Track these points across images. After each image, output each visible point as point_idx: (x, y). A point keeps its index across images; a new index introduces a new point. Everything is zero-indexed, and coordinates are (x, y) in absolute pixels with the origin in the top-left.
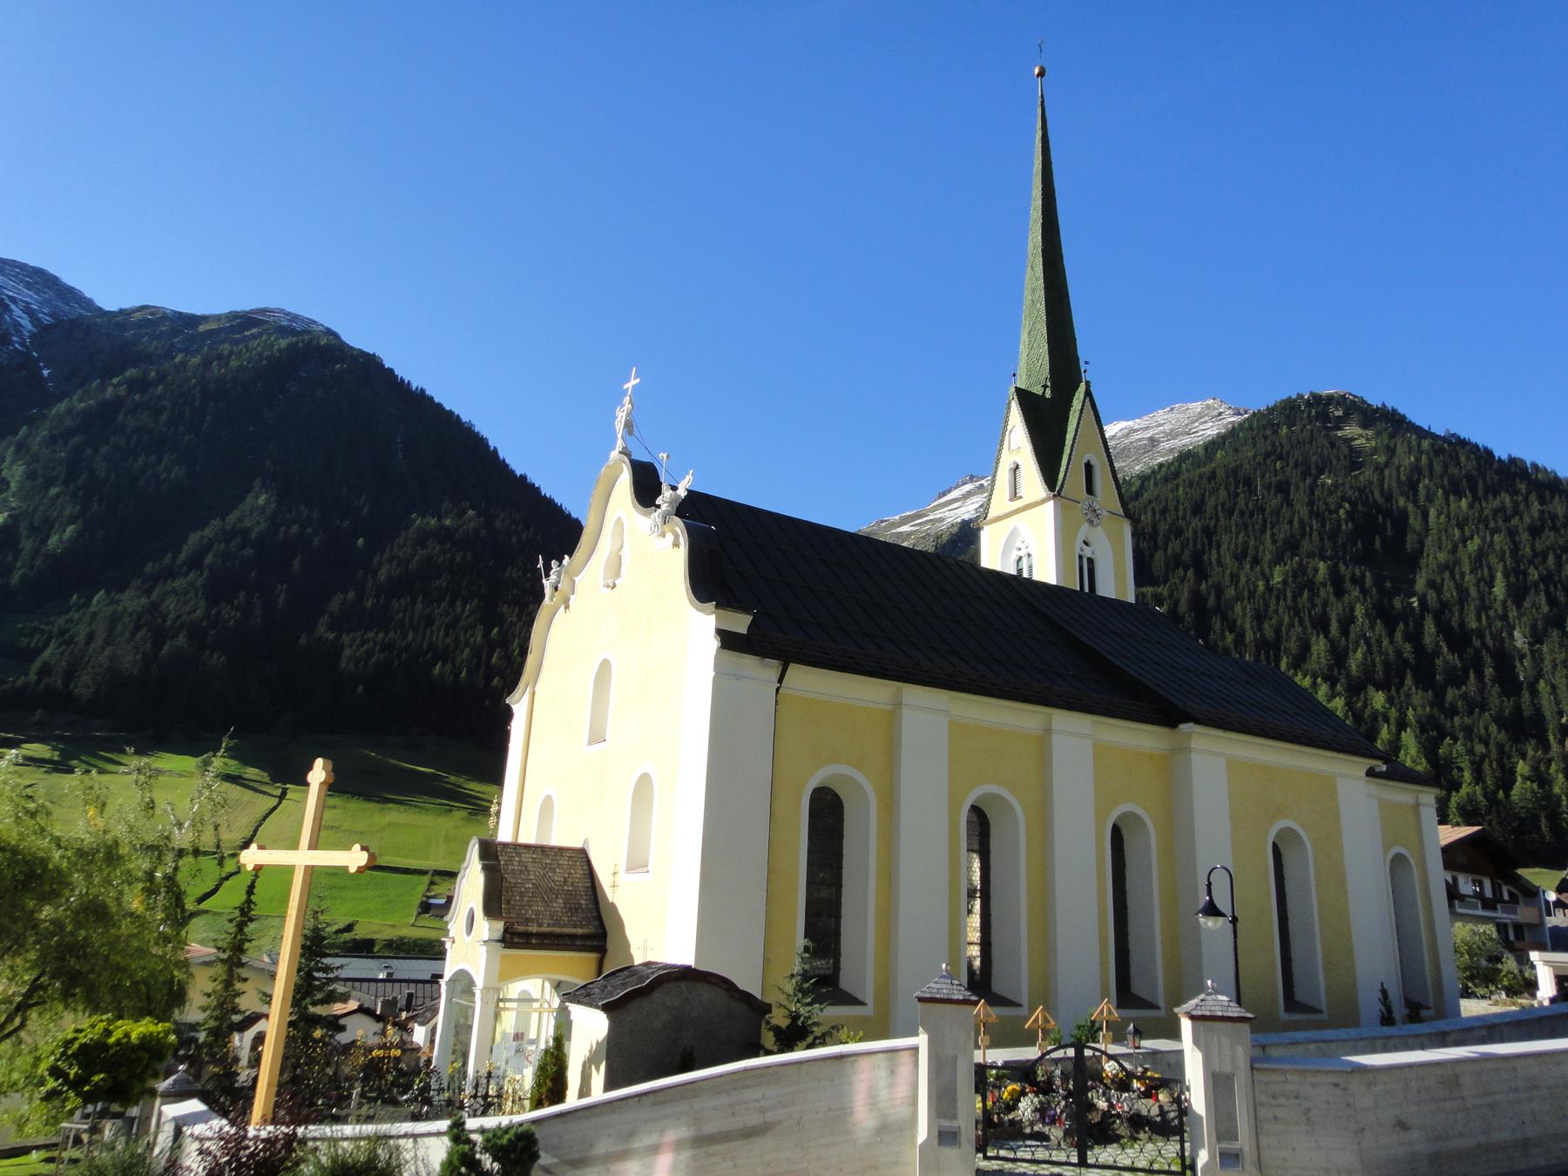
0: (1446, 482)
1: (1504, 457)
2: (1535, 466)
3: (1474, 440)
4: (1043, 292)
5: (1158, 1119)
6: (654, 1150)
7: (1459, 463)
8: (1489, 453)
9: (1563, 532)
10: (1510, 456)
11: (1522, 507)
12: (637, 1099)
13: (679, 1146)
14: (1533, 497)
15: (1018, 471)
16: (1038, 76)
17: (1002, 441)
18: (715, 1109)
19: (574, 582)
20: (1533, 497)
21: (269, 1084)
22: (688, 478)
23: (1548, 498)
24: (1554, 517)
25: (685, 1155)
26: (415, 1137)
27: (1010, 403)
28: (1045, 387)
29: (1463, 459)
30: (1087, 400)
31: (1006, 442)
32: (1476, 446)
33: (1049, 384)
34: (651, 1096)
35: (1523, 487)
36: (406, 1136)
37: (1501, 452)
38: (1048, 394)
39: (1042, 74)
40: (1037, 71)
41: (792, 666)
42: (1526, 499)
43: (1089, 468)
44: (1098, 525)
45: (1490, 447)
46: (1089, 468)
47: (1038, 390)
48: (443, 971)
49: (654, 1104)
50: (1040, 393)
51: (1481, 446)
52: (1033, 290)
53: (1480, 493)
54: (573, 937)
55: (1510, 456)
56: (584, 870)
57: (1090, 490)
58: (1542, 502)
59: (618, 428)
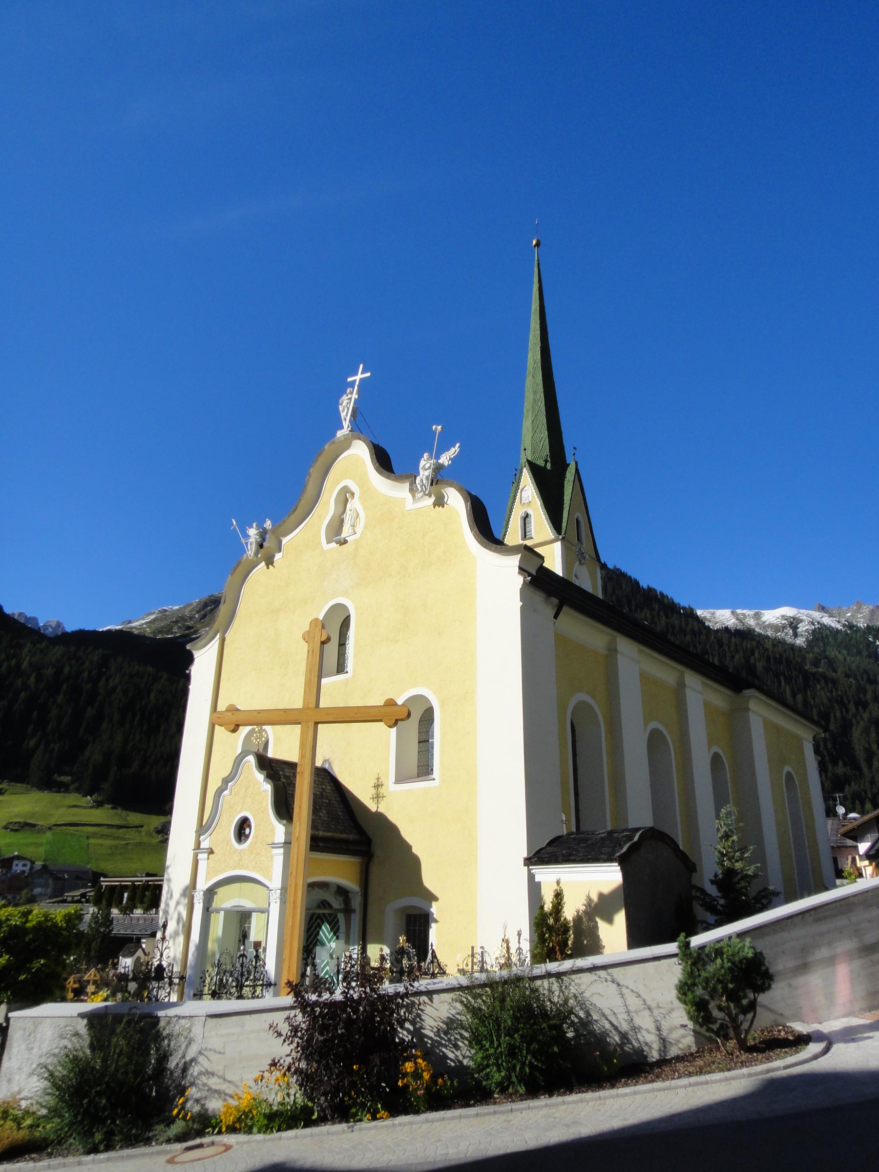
0: (614, 598)
1: (645, 587)
2: (662, 594)
3: (629, 574)
4: (542, 394)
5: (440, 1048)
6: (831, 961)
7: (621, 588)
8: (637, 583)
9: (678, 636)
10: (648, 586)
11: (656, 618)
12: (800, 916)
13: (850, 956)
14: (661, 613)
15: (527, 519)
16: (535, 246)
17: (515, 496)
18: (870, 921)
19: (280, 542)
20: (661, 613)
21: (299, 948)
22: (453, 450)
23: (670, 615)
24: (673, 627)
25: (857, 963)
26: (559, 975)
27: (522, 469)
28: (546, 461)
29: (624, 585)
30: (576, 477)
31: (518, 497)
32: (630, 577)
33: (549, 459)
34: (812, 913)
35: (656, 606)
36: (549, 975)
37: (644, 584)
38: (549, 466)
39: (538, 245)
40: (534, 242)
41: (565, 609)
42: (658, 615)
43: (578, 522)
44: (584, 564)
45: (638, 579)
46: (578, 522)
47: (541, 463)
48: (307, 860)
49: (817, 920)
50: (543, 465)
51: (633, 578)
52: (535, 392)
53: (633, 608)
54: (346, 842)
55: (648, 586)
56: (331, 787)
57: (579, 539)
58: (667, 617)
59: (343, 415)
